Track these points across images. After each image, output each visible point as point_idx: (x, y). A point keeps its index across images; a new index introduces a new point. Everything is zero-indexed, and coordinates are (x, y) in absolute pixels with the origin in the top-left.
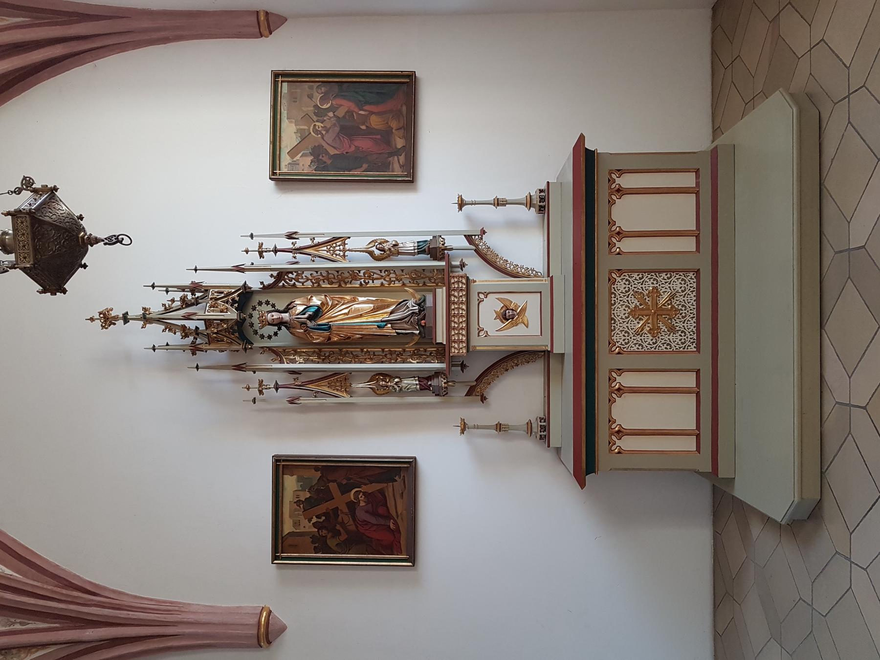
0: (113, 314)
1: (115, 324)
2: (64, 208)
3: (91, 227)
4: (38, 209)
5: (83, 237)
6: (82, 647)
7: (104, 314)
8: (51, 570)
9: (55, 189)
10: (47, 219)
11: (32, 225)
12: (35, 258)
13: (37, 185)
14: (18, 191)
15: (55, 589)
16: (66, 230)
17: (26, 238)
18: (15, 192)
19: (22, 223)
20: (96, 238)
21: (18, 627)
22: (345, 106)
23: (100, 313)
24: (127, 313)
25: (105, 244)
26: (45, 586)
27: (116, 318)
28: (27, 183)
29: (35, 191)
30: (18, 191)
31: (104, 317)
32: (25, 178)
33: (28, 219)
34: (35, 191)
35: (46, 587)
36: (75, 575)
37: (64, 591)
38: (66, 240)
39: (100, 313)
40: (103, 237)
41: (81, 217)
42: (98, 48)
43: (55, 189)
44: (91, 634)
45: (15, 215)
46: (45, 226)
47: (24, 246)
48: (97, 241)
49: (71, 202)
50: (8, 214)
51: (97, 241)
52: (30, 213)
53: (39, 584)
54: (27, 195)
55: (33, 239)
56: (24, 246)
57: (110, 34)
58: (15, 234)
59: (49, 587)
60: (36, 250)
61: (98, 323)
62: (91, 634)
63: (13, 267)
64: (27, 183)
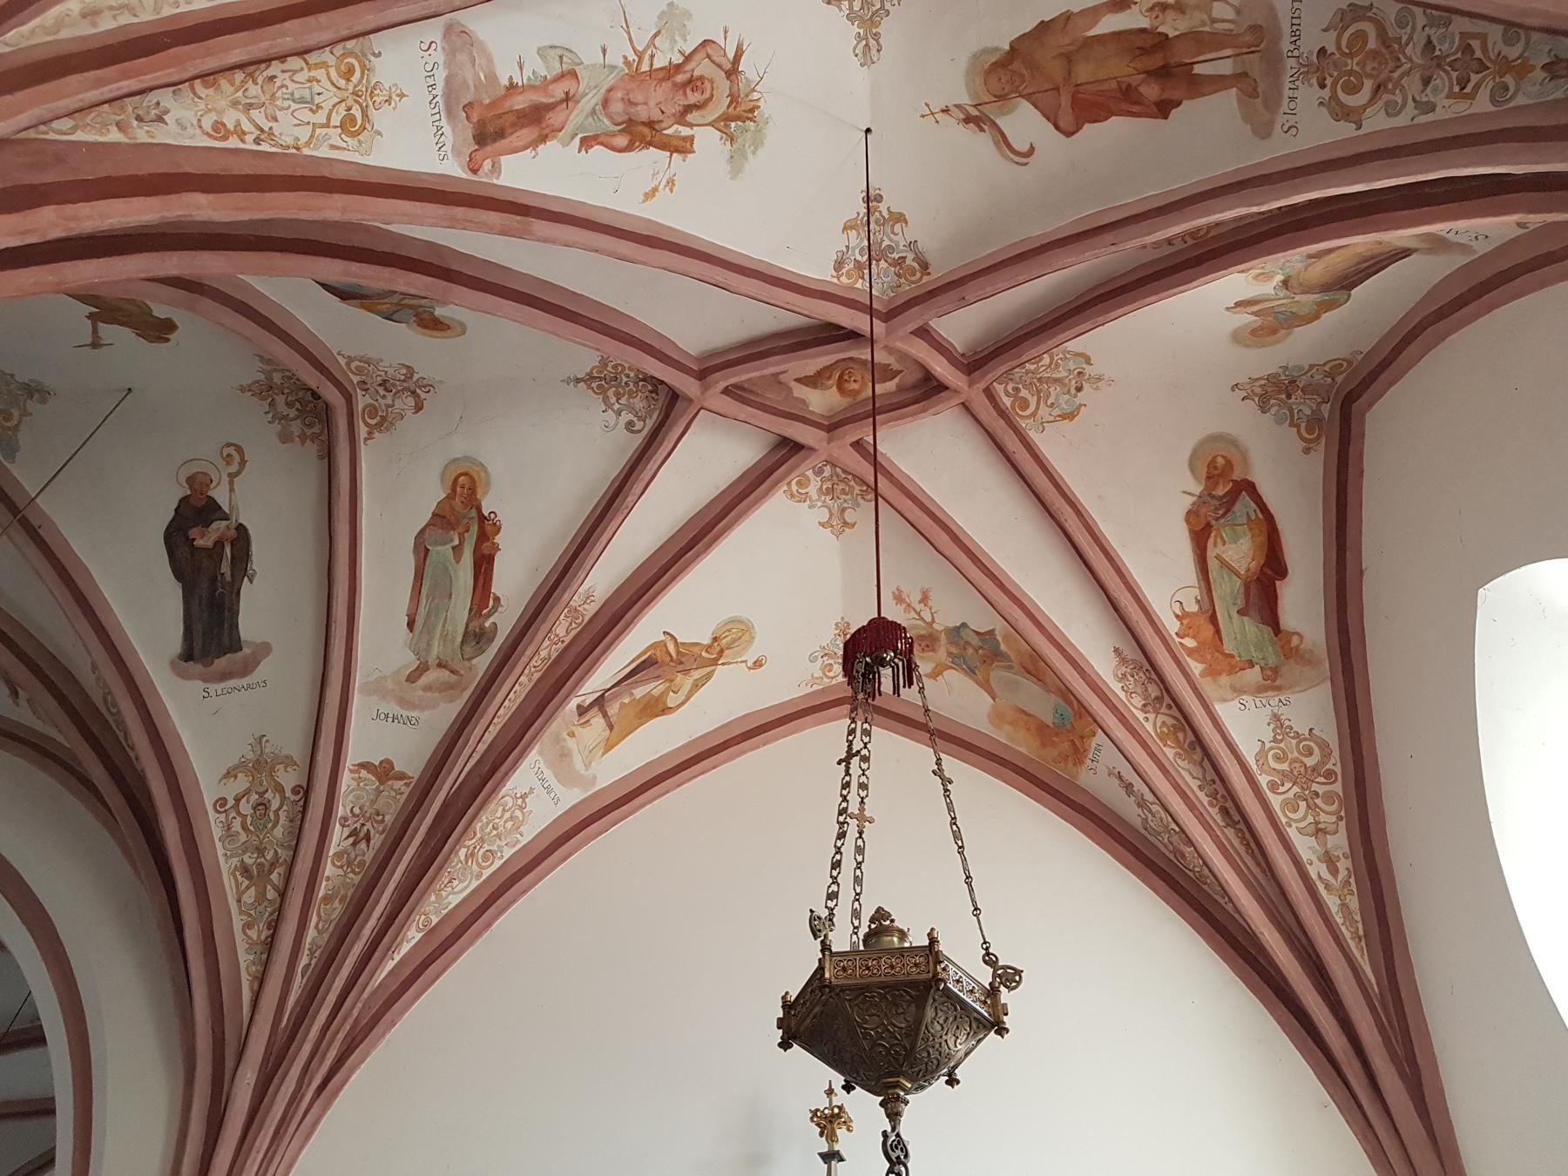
0: (841, 1132)
1: (821, 1134)
2: (962, 1048)
3: (926, 1108)
4: (948, 993)
5: (898, 1085)
6: (229, 1064)
7: (838, 1116)
8: (388, 1016)
9: (1002, 1031)
10: (930, 1013)
11: (914, 984)
12: (843, 989)
13: (1005, 995)
14: (989, 959)
15: (350, 1021)
16: (910, 1051)
17: (883, 970)
18: (988, 954)
19: (916, 965)
20: (898, 1114)
21: (304, 960)
22: (1380, 104)
23: (840, 1108)
24: (842, 1160)
25: (885, 1134)
26: (359, 1005)
27: (832, 1138)
28: (1009, 977)
29: (993, 992)
30: (989, 959)
31: (833, 1116)
32: (1019, 972)
33: (924, 976)
34: (993, 992)
35: (355, 1008)
36: (367, 1054)
37: (341, 1036)
38: (874, 1045)
39: (840, 1108)
40: (903, 1129)
41: (952, 1081)
42: (1360, 1106)
43: (1002, 1031)
44: (247, 1078)
45: (931, 951)
46: (913, 1008)
47: (868, 968)
48: (894, 1116)
49: (983, 1061)
50: (933, 940)
51: (894, 1116)
52: (936, 979)
53: (365, 995)
54: (985, 976)
55: (884, 986)
56: (868, 968)
57: (1392, 1120)
58: (902, 952)
59: (355, 1013)
60: (862, 990)
61: (822, 1103)
62: (247, 1078)
63: (825, 947)
64: (1009, 977)
